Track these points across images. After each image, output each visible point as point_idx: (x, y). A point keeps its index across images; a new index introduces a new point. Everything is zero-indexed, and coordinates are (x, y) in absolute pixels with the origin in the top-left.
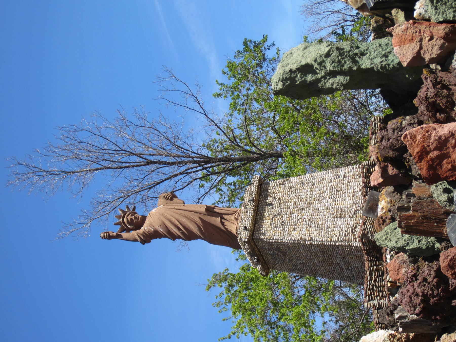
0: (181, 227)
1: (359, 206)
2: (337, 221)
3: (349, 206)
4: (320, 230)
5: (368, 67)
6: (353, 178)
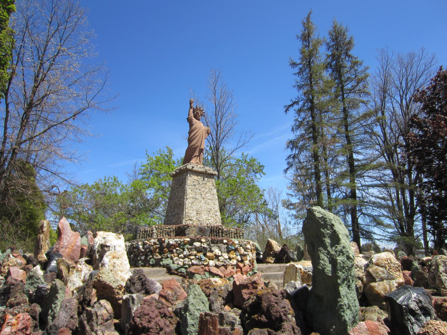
5: (341, 293)
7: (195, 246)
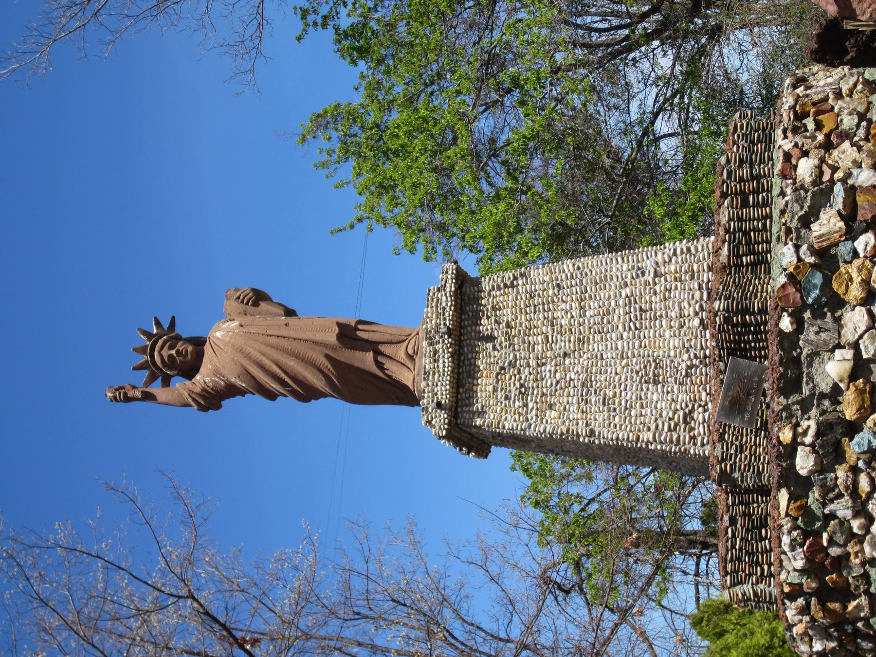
0: (287, 379)
1: (696, 357)
2: (648, 389)
3: (672, 353)
4: (609, 411)
6: (676, 279)
7: (811, 472)
